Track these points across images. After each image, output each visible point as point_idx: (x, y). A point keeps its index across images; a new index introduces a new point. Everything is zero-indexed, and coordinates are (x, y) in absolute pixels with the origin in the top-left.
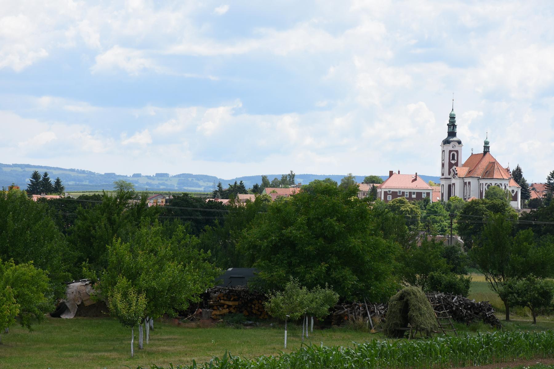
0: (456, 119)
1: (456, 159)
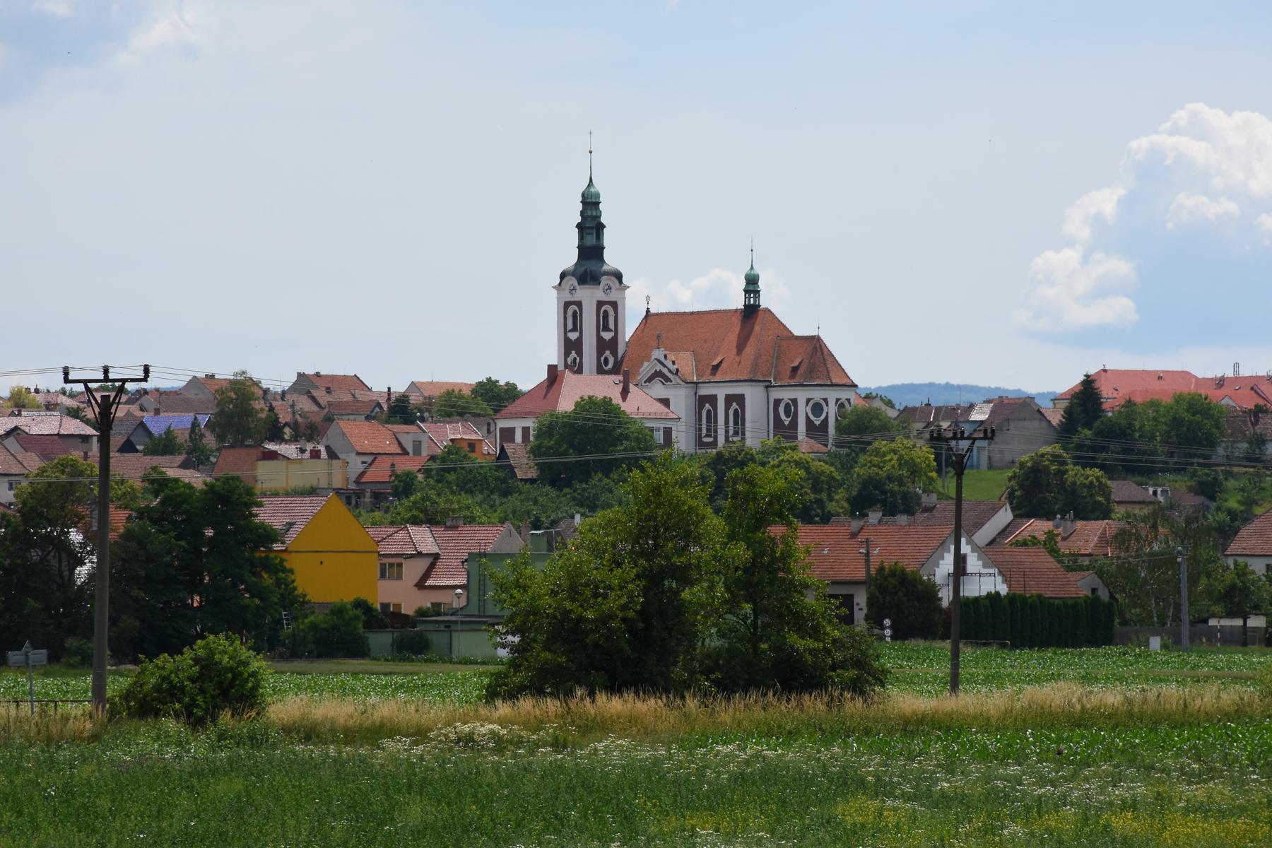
1: (612, 326)
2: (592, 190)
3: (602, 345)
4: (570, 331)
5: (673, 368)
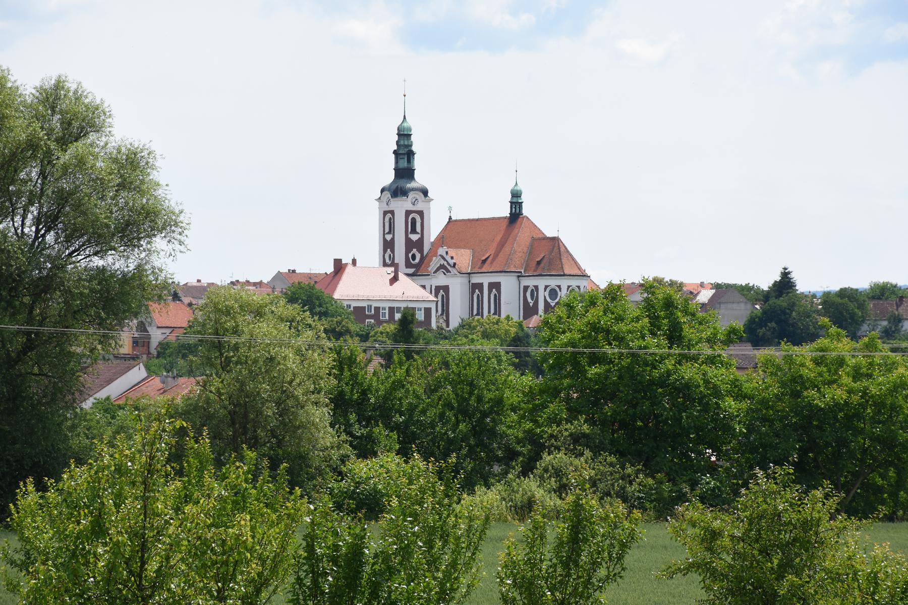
0: (413, 138)
1: (418, 229)
2: (405, 125)
3: (409, 245)
4: (387, 233)
5: (451, 262)
